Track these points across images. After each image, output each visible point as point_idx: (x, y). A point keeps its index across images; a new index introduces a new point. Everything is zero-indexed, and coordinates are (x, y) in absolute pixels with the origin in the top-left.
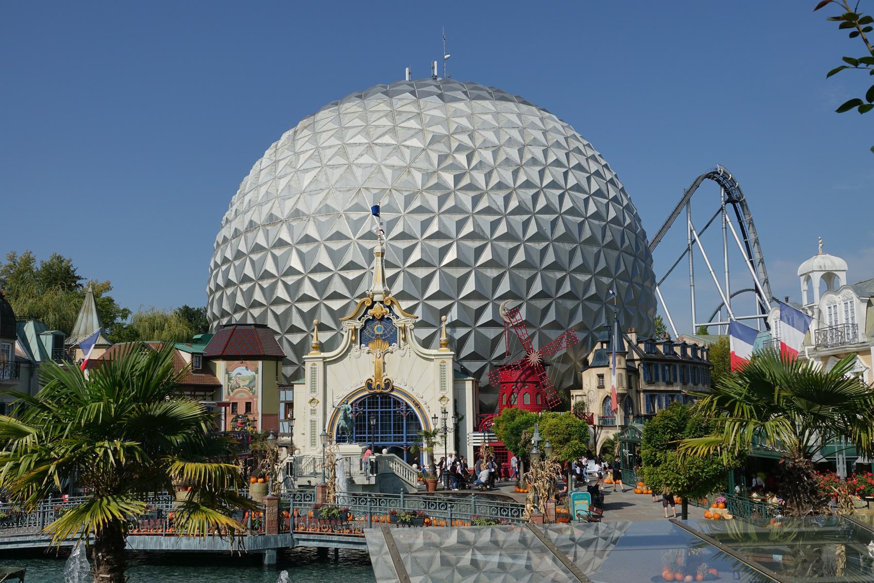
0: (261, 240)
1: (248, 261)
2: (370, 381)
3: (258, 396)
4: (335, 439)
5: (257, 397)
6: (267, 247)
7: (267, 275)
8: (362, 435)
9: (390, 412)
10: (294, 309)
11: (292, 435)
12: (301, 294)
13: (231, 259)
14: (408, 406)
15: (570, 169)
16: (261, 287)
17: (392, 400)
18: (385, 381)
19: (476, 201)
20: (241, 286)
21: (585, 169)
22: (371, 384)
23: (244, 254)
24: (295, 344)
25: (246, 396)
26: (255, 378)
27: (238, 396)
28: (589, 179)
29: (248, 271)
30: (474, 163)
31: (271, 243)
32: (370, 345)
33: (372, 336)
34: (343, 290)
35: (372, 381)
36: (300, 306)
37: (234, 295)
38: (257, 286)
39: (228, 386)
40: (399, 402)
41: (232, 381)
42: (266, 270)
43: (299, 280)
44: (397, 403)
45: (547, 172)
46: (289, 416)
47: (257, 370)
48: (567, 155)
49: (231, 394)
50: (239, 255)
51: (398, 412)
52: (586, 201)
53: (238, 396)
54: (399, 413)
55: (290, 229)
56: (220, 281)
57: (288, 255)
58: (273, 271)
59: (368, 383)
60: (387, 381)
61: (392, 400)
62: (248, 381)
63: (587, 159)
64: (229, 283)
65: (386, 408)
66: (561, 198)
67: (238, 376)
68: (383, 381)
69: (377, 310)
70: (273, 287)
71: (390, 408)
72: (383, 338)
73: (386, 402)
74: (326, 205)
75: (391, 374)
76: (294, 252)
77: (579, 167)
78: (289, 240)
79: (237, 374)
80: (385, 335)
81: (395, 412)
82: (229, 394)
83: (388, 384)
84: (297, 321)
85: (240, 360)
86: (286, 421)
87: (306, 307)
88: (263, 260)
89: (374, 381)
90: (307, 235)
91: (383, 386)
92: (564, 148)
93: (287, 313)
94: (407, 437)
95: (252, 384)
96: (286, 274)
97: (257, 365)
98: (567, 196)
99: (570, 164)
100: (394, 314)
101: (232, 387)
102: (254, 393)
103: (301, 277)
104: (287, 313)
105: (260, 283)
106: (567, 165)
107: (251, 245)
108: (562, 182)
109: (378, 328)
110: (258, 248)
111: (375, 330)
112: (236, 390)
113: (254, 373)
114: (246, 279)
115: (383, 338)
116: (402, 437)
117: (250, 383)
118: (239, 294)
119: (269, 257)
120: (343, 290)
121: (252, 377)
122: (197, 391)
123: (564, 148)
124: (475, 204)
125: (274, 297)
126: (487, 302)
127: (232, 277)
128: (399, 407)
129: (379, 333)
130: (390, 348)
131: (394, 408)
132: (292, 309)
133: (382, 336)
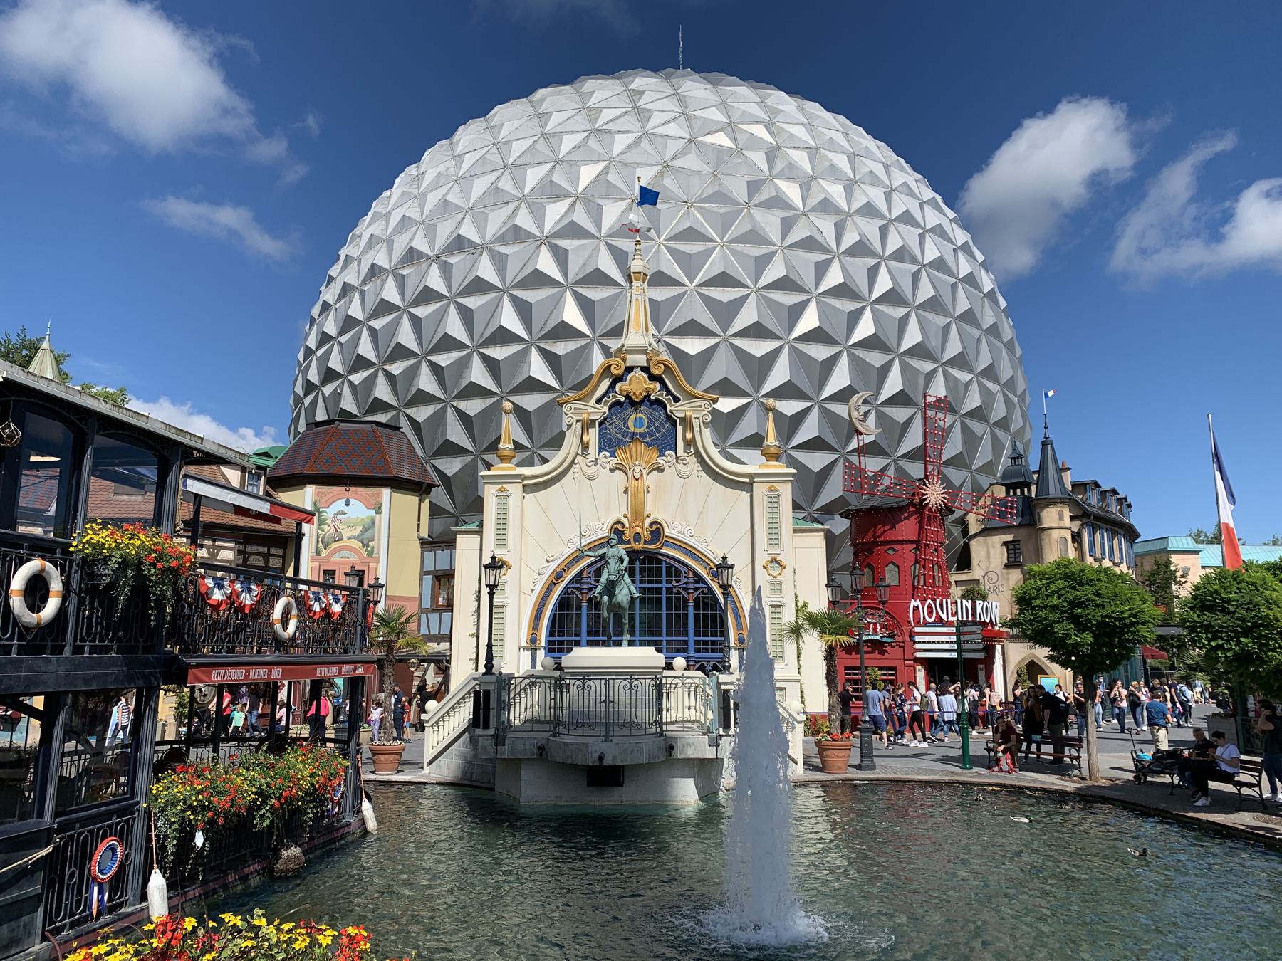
0: (391, 293)
1: (365, 333)
2: (619, 527)
3: (378, 558)
4: (543, 644)
5: (377, 561)
6: (401, 305)
7: (400, 352)
8: (710, 638)
9: (659, 591)
10: (450, 411)
11: (449, 638)
12: (464, 383)
13: (334, 335)
14: (698, 578)
15: (892, 221)
16: (389, 375)
17: (664, 565)
18: (651, 526)
19: (787, 226)
20: (351, 378)
21: (915, 219)
22: (623, 533)
23: (357, 322)
24: (450, 475)
25: (353, 558)
26: (374, 523)
27: (336, 557)
28: (922, 237)
29: (366, 348)
30: (779, 166)
31: (409, 296)
32: (620, 454)
33: (623, 435)
34: (485, 380)
35: (623, 526)
36: (463, 405)
37: (337, 395)
38: (381, 374)
39: (318, 538)
40: (677, 571)
41: (326, 528)
42: (398, 344)
43: (461, 358)
44: (674, 571)
45: (849, 225)
46: (441, 601)
47: (380, 508)
48: (888, 196)
49: (324, 553)
50: (349, 323)
51: (675, 591)
52: (915, 277)
53: (336, 557)
54: (679, 593)
55: (446, 270)
56: (313, 376)
57: (441, 315)
58: (412, 345)
59: (616, 529)
60: (655, 527)
61: (664, 565)
62: (360, 528)
63: (921, 205)
64: (329, 375)
65: (650, 582)
66: (873, 273)
67: (340, 516)
68: (646, 525)
69: (637, 384)
70: (412, 373)
71: (659, 582)
72: (648, 439)
73: (650, 569)
74: (515, 226)
75: (655, 510)
76: (452, 308)
77: (907, 218)
78: (443, 290)
79: (337, 514)
80: (651, 434)
81: (669, 590)
82: (318, 553)
83: (657, 532)
84: (455, 433)
85: (346, 485)
86: (433, 611)
87: (473, 407)
88: (394, 327)
89: (627, 525)
90: (477, 278)
91: (647, 535)
92: (883, 185)
93: (438, 418)
94: (697, 642)
95: (367, 535)
96: (437, 349)
97: (380, 496)
98: (883, 269)
99: (893, 211)
100: (669, 392)
101: (326, 540)
102: (370, 553)
103: (464, 353)
104: (438, 418)
105: (387, 367)
106: (887, 214)
107: (371, 303)
108: (877, 245)
109: (636, 421)
110: (384, 308)
111: (630, 424)
112: (334, 546)
113: (372, 513)
114: (360, 363)
115: (648, 439)
116: (686, 642)
117: (363, 532)
118: (347, 391)
119: (406, 320)
120: (485, 380)
121: (369, 521)
122: (252, 544)
123: (883, 185)
124: (785, 231)
125: (414, 390)
126: (809, 404)
127: (336, 363)
128: (678, 581)
129: (637, 430)
130: (661, 460)
131: (668, 582)
132: (446, 411)
133: (643, 435)
